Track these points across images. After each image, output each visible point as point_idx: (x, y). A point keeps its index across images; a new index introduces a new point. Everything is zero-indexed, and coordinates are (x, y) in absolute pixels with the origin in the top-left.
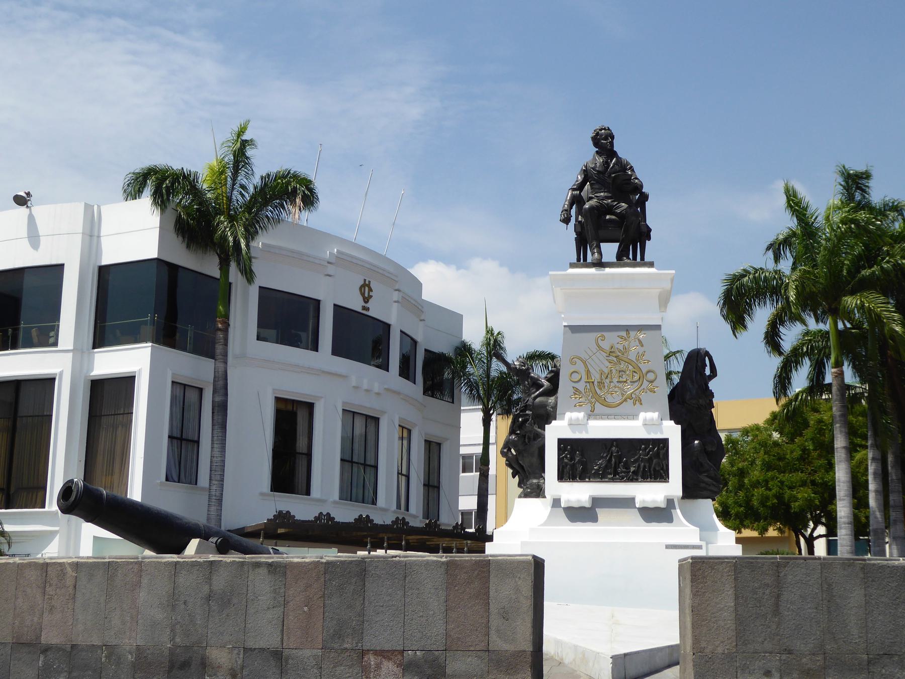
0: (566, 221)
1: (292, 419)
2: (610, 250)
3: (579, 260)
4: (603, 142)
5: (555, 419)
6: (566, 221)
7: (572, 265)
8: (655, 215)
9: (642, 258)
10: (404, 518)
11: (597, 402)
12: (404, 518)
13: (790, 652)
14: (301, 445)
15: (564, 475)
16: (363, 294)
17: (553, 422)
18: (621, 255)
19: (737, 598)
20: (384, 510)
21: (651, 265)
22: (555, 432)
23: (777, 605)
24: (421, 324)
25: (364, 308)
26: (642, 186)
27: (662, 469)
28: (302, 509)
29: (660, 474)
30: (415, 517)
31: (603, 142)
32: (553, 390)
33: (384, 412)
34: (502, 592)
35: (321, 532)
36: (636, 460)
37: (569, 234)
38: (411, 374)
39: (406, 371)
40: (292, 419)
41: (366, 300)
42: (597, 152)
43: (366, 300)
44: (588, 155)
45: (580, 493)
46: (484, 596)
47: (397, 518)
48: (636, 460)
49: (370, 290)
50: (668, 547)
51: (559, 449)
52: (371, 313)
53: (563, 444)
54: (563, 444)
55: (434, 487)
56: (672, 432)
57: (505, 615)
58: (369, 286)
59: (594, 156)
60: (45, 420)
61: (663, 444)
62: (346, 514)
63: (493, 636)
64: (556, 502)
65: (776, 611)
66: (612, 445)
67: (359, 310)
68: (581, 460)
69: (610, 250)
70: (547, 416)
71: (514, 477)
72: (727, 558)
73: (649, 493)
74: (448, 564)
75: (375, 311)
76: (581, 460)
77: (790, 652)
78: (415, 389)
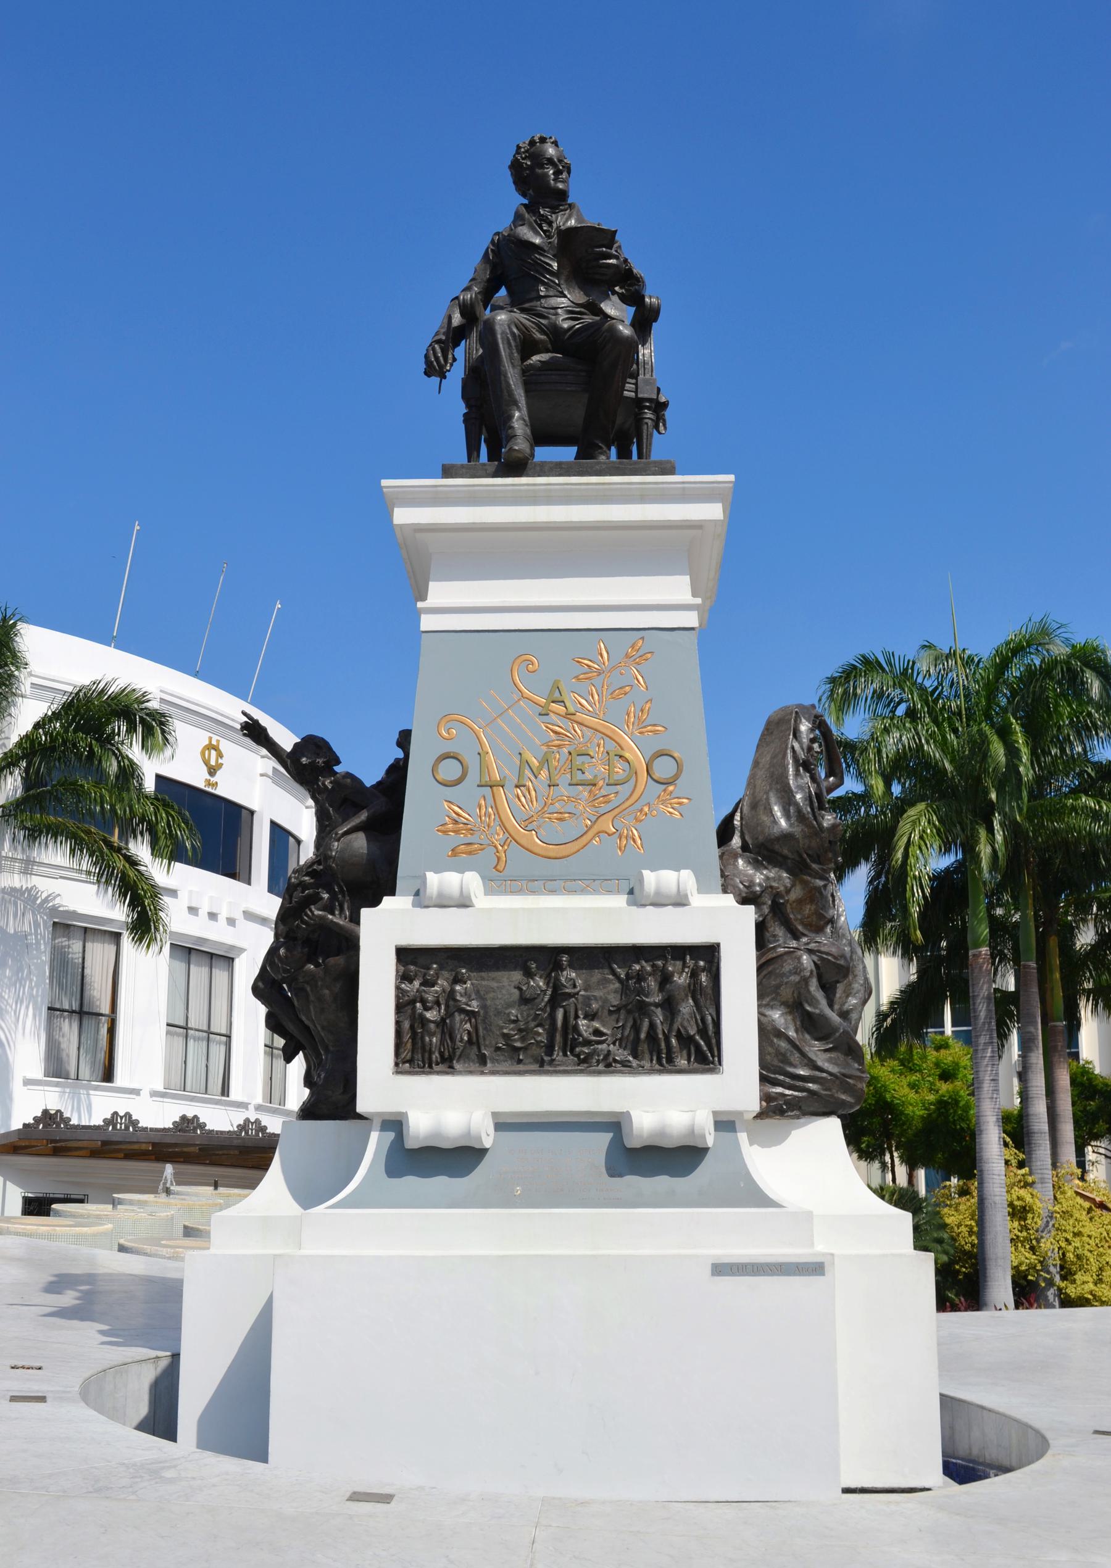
0: (435, 369)
4: (536, 179)
6: (435, 369)
15: (418, 1051)
16: (206, 763)
17: (387, 900)
22: (385, 930)
25: (208, 783)
27: (703, 1032)
28: (94, 1108)
29: (703, 1052)
31: (536, 179)
32: (1067, 1302)
33: (242, 950)
36: (649, 1006)
38: (240, 866)
41: (212, 771)
43: (212, 771)
44: (500, 207)
45: (451, 1105)
48: (649, 1006)
49: (220, 755)
50: (720, 1269)
52: (220, 791)
54: (410, 958)
56: (728, 926)
58: (216, 748)
61: (709, 954)
64: (395, 1124)
67: (201, 785)
68: (484, 1008)
70: (376, 881)
73: (661, 1103)
76: (484, 1008)
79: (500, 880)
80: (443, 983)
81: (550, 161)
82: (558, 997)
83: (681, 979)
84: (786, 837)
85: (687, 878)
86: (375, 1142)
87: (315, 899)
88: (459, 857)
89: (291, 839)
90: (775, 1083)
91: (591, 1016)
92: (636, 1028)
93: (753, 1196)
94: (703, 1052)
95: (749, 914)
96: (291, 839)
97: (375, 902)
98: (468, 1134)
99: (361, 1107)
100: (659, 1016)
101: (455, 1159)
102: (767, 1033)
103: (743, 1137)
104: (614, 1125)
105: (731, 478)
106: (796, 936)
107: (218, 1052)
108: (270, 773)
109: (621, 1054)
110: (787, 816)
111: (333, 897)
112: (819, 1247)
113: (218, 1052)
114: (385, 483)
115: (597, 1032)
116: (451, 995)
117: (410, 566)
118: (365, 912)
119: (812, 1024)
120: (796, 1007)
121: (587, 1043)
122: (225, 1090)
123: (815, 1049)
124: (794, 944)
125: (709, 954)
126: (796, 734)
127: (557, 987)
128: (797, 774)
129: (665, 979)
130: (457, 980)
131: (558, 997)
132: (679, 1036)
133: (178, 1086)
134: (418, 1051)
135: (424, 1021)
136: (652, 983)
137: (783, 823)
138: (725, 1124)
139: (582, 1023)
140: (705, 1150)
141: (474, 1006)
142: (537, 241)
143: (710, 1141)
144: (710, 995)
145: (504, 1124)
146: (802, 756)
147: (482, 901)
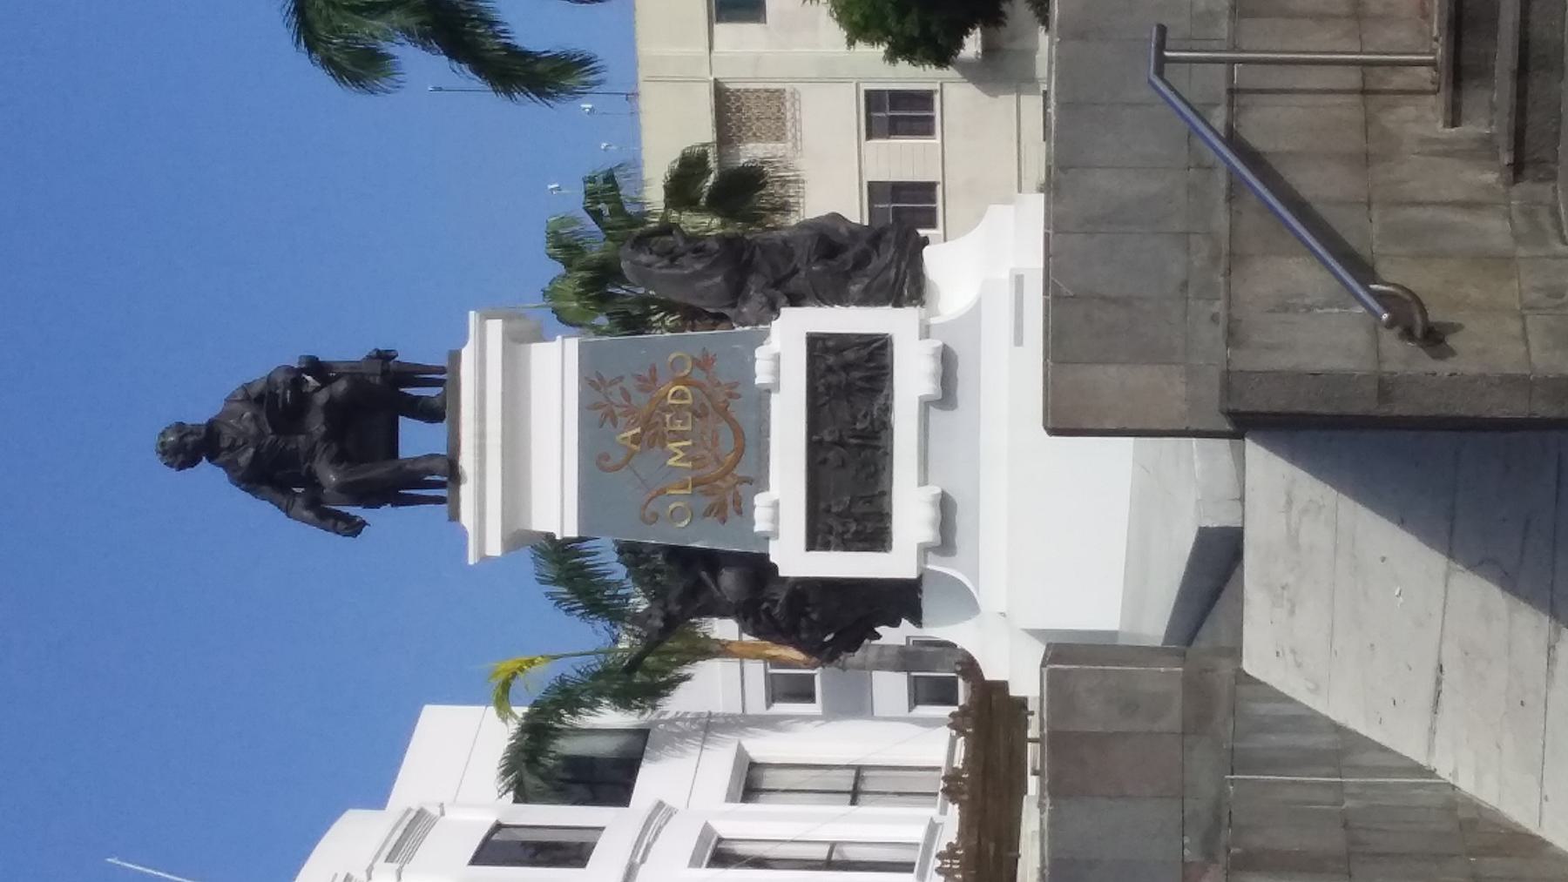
0: (354, 528)
2: (415, 438)
3: (440, 500)
4: (190, 447)
5: (767, 556)
7: (455, 516)
8: (347, 347)
9: (442, 370)
10: (940, 856)
11: (734, 475)
12: (940, 856)
13: (1185, 284)
15: (875, 536)
17: (772, 559)
19: (1106, 362)
22: (794, 558)
23: (1115, 301)
24: (451, 815)
26: (289, 369)
30: (933, 829)
31: (190, 447)
33: (707, 830)
37: (382, 520)
42: (210, 460)
45: (911, 514)
46: (1101, 741)
47: (939, 871)
51: (826, 547)
53: (817, 539)
54: (817, 539)
55: (858, 778)
59: (220, 465)
61: (818, 345)
63: (1163, 725)
64: (925, 550)
66: (821, 442)
69: (415, 438)
70: (759, 568)
71: (879, 637)
72: (1045, 376)
73: (911, 378)
77: (1185, 284)
79: (759, 481)
80: (832, 521)
81: (181, 438)
82: (840, 443)
83: (831, 360)
84: (727, 279)
85: (760, 353)
86: (936, 565)
87: (768, 611)
88: (743, 509)
89: (495, 837)
90: (901, 293)
91: (855, 420)
92: (861, 390)
93: (974, 316)
95: (787, 312)
96: (495, 837)
97: (774, 568)
98: (933, 504)
99: (913, 575)
100: (856, 374)
101: (946, 507)
103: (933, 321)
104: (926, 405)
105: (472, 313)
106: (795, 271)
108: (396, 866)
109: (881, 400)
110: (710, 277)
111: (765, 600)
112: (1005, 275)
114: (471, 562)
115: (865, 416)
116: (839, 515)
117: (484, 559)
118: (781, 574)
119: (861, 262)
120: (847, 277)
121: (872, 423)
123: (876, 263)
124: (803, 273)
125: (818, 345)
126: (649, 265)
127: (835, 443)
128: (681, 267)
129: (830, 369)
130: (828, 511)
131: (840, 443)
132: (868, 361)
134: (875, 536)
135: (856, 532)
136: (832, 379)
137: (718, 279)
138: (926, 332)
139: (859, 426)
140: (945, 346)
141: (847, 499)
142: (251, 451)
143: (939, 343)
144: (842, 343)
145: (924, 481)
146: (666, 262)
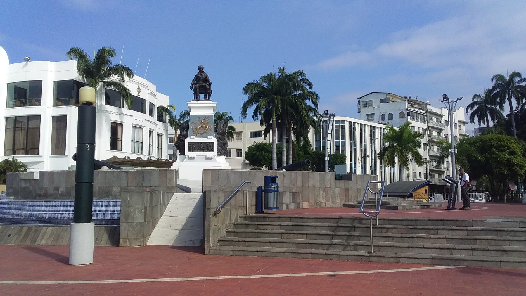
0: (191, 89)
1: (115, 129)
2: (202, 96)
4: (201, 69)
8: (212, 88)
14: (119, 136)
18: (205, 98)
20: (145, 157)
21: (211, 101)
22: (187, 140)
28: (120, 155)
29: (212, 150)
30: (154, 157)
31: (201, 69)
34: (169, 176)
35: (127, 162)
36: (209, 147)
39: (151, 114)
40: (115, 129)
46: (166, 177)
57: (170, 180)
60: (38, 129)
61: (213, 143)
62: (133, 157)
64: (189, 156)
65: (218, 179)
68: (194, 147)
70: (186, 136)
73: (209, 154)
74: (159, 171)
75: (142, 96)
76: (194, 147)
78: (154, 119)
88: (193, 134)
93: (216, 161)
94: (212, 150)
102: (218, 149)
107: (140, 145)
113: (140, 145)
119: (223, 148)
122: (142, 153)
125: (213, 143)
133: (133, 152)
138: (214, 156)
147: (195, 138)
